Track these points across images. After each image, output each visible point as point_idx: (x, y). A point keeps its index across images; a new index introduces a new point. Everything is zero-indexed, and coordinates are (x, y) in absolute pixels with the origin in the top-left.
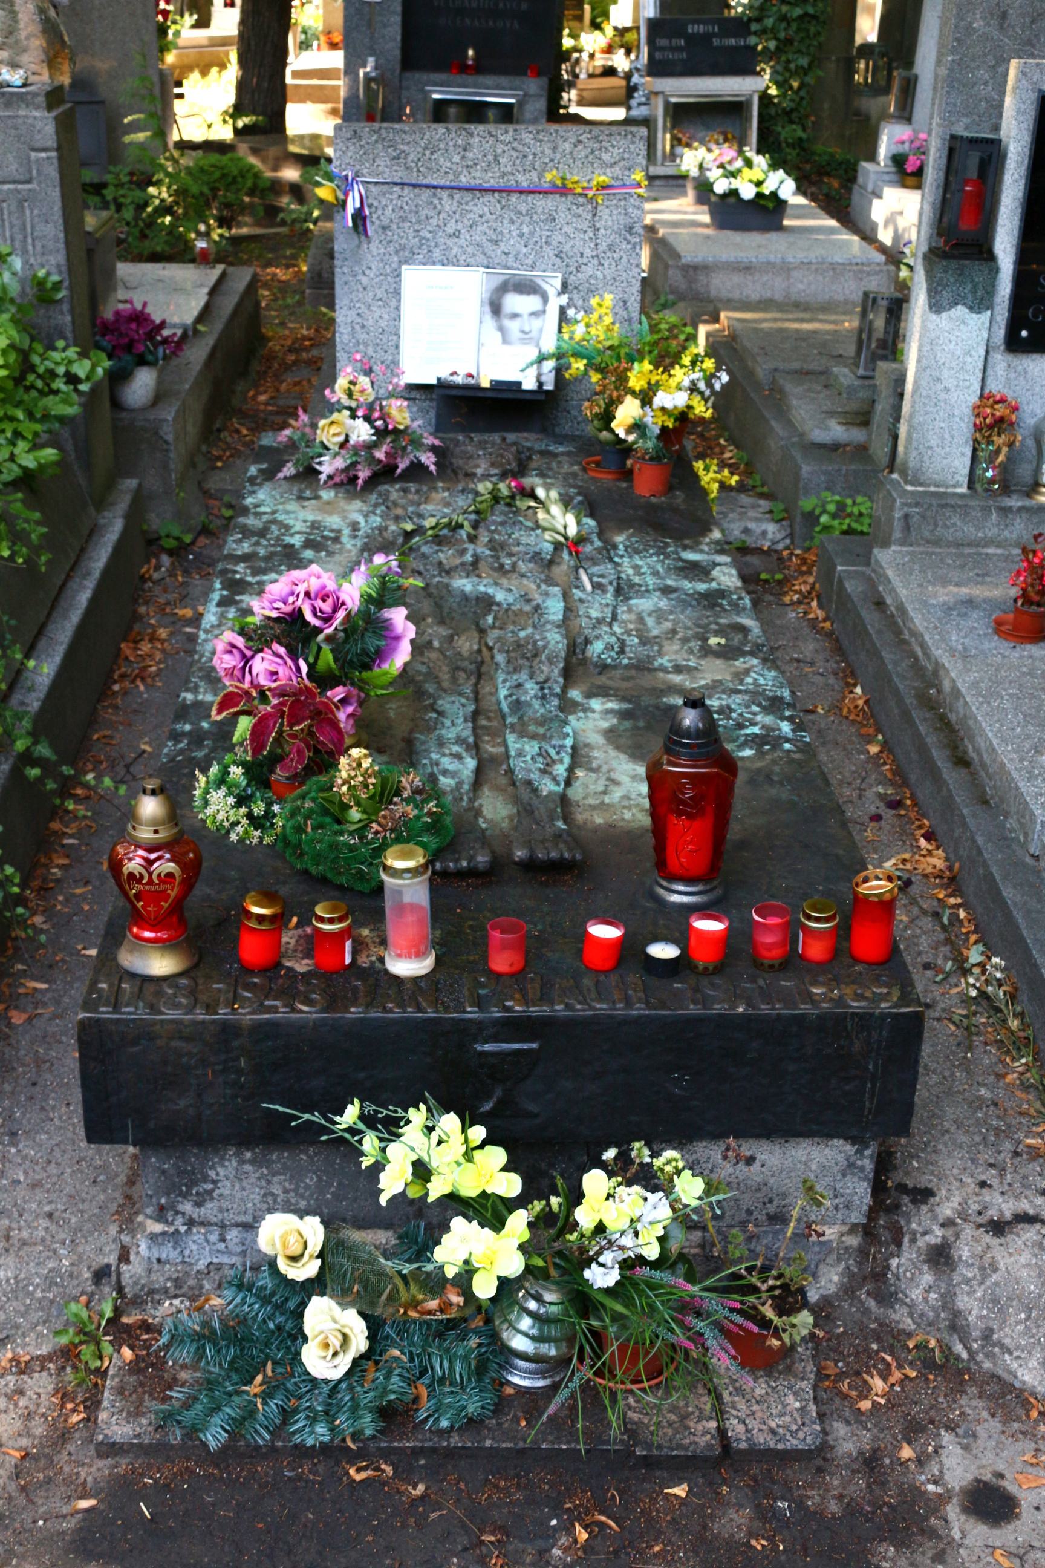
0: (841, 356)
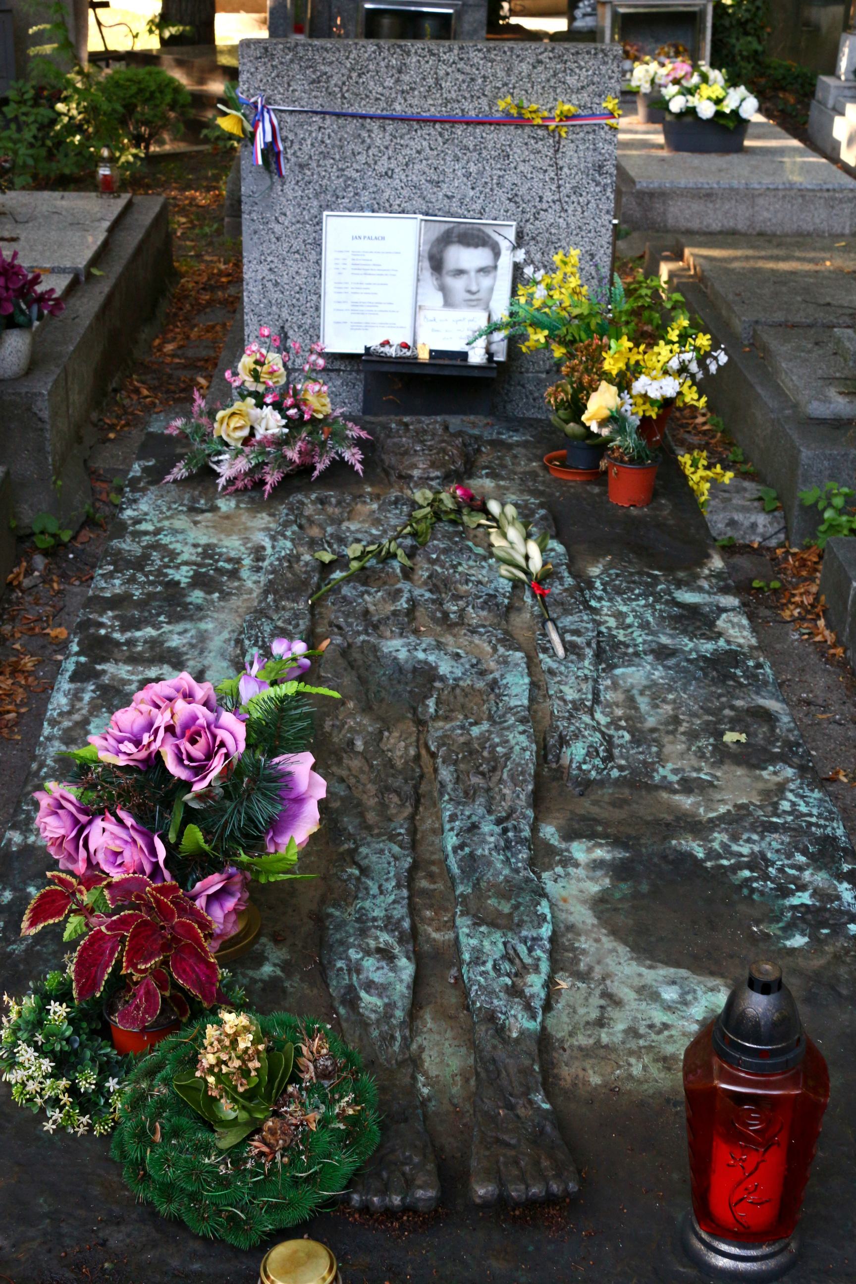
0: (829, 304)
